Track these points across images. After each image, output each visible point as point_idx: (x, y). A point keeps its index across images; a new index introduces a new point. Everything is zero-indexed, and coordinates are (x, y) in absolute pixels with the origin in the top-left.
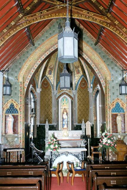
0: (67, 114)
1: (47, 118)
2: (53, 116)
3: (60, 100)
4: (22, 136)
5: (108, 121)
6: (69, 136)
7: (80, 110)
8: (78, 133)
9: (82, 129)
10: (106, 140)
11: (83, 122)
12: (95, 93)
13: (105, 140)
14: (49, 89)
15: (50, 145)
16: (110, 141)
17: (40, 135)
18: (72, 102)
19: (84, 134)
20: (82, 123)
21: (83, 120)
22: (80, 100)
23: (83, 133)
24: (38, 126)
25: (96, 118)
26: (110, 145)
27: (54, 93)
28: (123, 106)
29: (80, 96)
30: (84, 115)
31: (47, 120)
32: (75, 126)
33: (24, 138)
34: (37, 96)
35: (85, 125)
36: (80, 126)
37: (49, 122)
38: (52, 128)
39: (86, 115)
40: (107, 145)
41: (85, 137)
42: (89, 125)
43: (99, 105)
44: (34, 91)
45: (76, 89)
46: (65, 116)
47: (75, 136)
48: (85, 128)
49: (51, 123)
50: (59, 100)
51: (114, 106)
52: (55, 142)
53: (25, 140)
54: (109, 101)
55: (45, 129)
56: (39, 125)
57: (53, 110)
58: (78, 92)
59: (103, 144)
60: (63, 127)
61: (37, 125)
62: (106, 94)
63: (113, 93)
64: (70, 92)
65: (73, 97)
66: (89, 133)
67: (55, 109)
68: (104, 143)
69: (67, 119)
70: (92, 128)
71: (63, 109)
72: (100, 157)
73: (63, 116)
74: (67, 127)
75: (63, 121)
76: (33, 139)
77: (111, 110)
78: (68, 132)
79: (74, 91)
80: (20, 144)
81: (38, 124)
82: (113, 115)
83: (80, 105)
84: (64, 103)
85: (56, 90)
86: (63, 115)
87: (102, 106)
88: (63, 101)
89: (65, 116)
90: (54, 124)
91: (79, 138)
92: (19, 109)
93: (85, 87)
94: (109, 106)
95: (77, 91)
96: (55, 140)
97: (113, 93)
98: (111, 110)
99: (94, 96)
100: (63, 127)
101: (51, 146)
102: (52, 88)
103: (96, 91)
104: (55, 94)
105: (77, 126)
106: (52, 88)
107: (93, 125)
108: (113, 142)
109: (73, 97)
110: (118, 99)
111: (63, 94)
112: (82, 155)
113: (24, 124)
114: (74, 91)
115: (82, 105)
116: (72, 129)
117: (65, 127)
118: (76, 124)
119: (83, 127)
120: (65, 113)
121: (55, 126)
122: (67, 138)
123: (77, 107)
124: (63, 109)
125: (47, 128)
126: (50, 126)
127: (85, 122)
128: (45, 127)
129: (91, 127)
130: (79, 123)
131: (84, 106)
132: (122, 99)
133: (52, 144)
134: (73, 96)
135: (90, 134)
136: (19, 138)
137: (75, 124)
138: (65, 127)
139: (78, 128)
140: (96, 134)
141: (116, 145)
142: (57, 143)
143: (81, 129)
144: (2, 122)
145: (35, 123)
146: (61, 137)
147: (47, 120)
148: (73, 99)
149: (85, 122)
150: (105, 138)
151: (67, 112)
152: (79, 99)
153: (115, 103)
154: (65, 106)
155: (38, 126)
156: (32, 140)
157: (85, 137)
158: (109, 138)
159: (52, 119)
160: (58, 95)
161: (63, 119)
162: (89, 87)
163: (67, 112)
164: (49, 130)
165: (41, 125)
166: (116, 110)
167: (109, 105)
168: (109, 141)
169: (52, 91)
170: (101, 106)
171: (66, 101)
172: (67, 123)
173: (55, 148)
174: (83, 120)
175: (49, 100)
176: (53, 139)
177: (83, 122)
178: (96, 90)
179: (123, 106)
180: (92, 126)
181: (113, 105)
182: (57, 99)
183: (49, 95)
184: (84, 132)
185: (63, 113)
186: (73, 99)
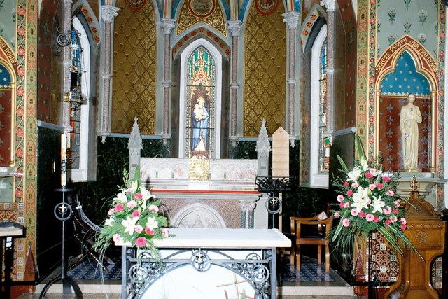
0: (207, 104)
1: (139, 113)
2: (160, 107)
3: (185, 54)
4: (24, 175)
5: (368, 123)
6: (213, 177)
7: (253, 91)
8: (246, 171)
9: (259, 156)
10: (368, 200)
11: (263, 129)
12: (309, 30)
13: (361, 199)
14: (148, 15)
15: (123, 217)
16: (383, 204)
17: (112, 173)
18: (226, 65)
19: (265, 174)
20: (257, 134)
21: (264, 122)
22: (253, 54)
23: (263, 168)
24: (103, 140)
25: (307, 118)
26: (381, 218)
27: (163, 28)
28: (426, 66)
29: (253, 40)
30: (265, 108)
31: (136, 119)
32: (234, 144)
33: (35, 182)
34: (100, 34)
35: (271, 142)
36: (253, 145)
37: (144, 127)
38: (152, 149)
39: (272, 109)
40: (370, 218)
41: (268, 185)
42: (283, 141)
43: (321, 73)
44: (91, 13)
45: (241, 18)
46: (200, 112)
47: (232, 177)
48: (269, 150)
49: (150, 132)
50: (180, 57)
51: (393, 65)
52: (144, 206)
53: (39, 191)
54: (373, 48)
55: (128, 150)
56: (108, 138)
57: (161, 88)
58: (247, 29)
59: (350, 215)
60: (192, 149)
61: (100, 138)
62: (363, 16)
63: (392, 16)
64: (219, 27)
65: (231, 46)
66: (282, 170)
67: (167, 86)
68: (357, 211)
69: (206, 121)
70: (294, 153)
71: (194, 88)
72: (319, 256)
73: (193, 111)
74: (207, 147)
75: (193, 127)
76: (67, 186)
77: (379, 79)
78: (207, 162)
79: (234, 25)
80: (15, 205)
81: (104, 133)
82: (385, 102)
83: (253, 72)
84: (197, 68)
85: (173, 17)
86: (193, 108)
87: (341, 70)
88: (196, 59)
89: (200, 112)
90: (163, 135)
91: (252, 188)
92: (15, 68)
93: (274, 8)
94: (372, 66)
95: (244, 25)
96: (146, 195)
97: (392, 16)
98: (379, 79)
99: (305, 39)
100: (192, 148)
101: (124, 223)
102: (157, 11)
103: (313, 22)
104: (168, 32)
105: (240, 144)
106: (157, 11)
107: (297, 142)
108: (393, 207)
109: (231, 46)
110: (409, 39)
111: (195, 35)
112: (268, 265)
113: (34, 126)
114: (234, 25)
115: (259, 74)
116: (225, 155)
117: (201, 147)
118: (236, 137)
119: (262, 148)
120: (201, 101)
121: (165, 143)
122: (205, 186)
123: (241, 81)
124: (194, 88)
125: (135, 148)
126: (145, 142)
127: (270, 134)
128: (129, 144)
129: (290, 147)
130: (247, 134)
131: (266, 77)
132: (423, 41)
133: (131, 212)
134: (228, 42)
135: (286, 174)
136: (11, 184)
137: (232, 137)
138: (201, 147)
139: (247, 151)
140: (307, 174)
141: (404, 220)
142: (154, 207)
143: (253, 155)
144: (20, 128)
145: (95, 130)
146: (185, 182)
147: (136, 119)
148: (228, 52)
149: (270, 134)
150: (360, 188)
151: (206, 97)
152: (251, 53)
153: (396, 54)
154: (201, 77)
155: (103, 140)
156: (64, 190)
157: (268, 185)
158: (377, 192)
159: (153, 117)
160: (177, 38)
161: (193, 118)
162: (289, 9)
163: (206, 97)
164: (143, 155)
165: (116, 138)
166: (396, 85)
167: (372, 59)
168: (379, 205)
169: (158, 23)
170: (331, 71)
171: (206, 60)
172: (208, 135)
173: (142, 235)
174: (263, 125)
175: (146, 51)
176: (138, 191)
177: (263, 129)
178: (313, 17)
179: (426, 66)
180: (293, 145)
181: (389, 64)
182: (174, 50)
183: (147, 34)
184: (265, 164)
185: (195, 102)
186: (228, 52)
